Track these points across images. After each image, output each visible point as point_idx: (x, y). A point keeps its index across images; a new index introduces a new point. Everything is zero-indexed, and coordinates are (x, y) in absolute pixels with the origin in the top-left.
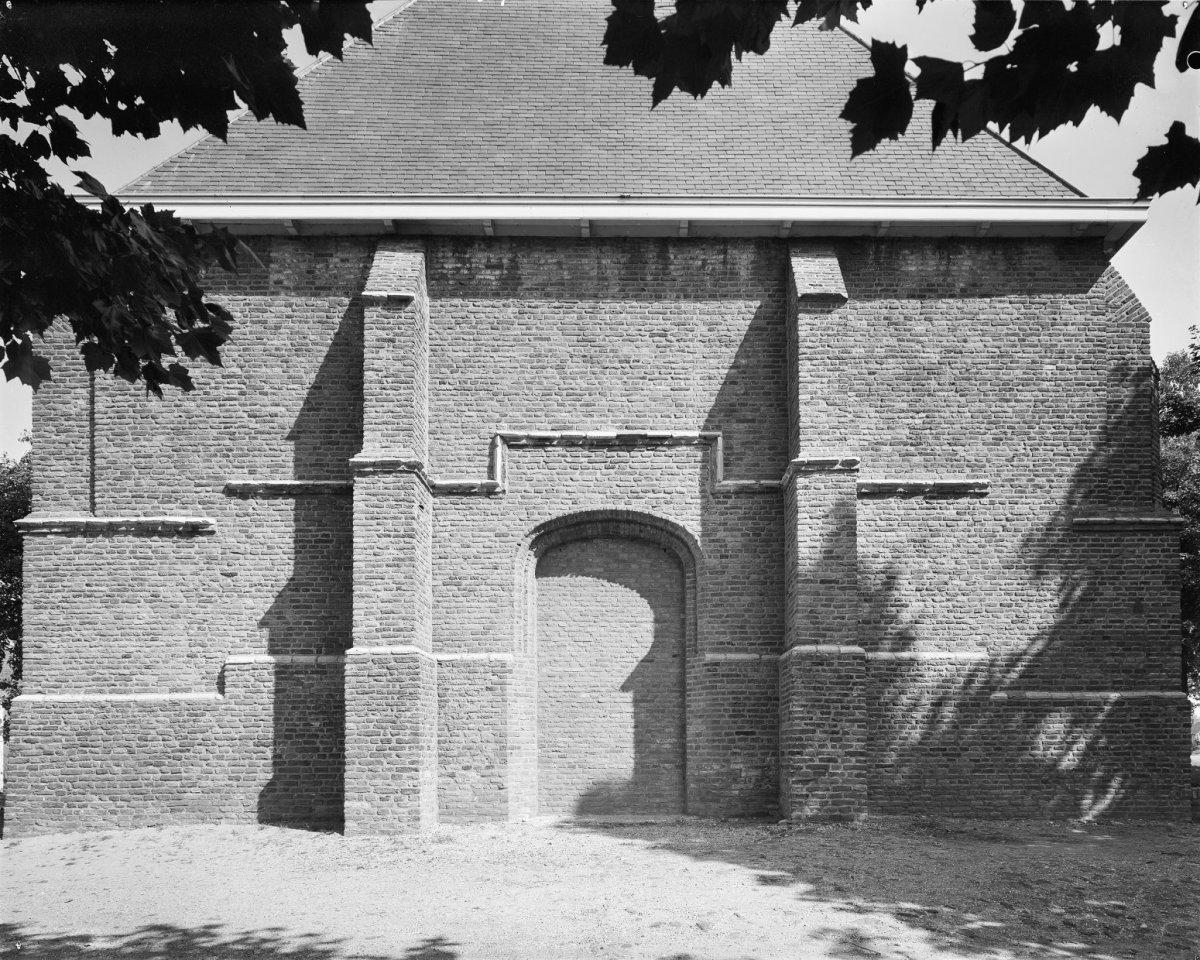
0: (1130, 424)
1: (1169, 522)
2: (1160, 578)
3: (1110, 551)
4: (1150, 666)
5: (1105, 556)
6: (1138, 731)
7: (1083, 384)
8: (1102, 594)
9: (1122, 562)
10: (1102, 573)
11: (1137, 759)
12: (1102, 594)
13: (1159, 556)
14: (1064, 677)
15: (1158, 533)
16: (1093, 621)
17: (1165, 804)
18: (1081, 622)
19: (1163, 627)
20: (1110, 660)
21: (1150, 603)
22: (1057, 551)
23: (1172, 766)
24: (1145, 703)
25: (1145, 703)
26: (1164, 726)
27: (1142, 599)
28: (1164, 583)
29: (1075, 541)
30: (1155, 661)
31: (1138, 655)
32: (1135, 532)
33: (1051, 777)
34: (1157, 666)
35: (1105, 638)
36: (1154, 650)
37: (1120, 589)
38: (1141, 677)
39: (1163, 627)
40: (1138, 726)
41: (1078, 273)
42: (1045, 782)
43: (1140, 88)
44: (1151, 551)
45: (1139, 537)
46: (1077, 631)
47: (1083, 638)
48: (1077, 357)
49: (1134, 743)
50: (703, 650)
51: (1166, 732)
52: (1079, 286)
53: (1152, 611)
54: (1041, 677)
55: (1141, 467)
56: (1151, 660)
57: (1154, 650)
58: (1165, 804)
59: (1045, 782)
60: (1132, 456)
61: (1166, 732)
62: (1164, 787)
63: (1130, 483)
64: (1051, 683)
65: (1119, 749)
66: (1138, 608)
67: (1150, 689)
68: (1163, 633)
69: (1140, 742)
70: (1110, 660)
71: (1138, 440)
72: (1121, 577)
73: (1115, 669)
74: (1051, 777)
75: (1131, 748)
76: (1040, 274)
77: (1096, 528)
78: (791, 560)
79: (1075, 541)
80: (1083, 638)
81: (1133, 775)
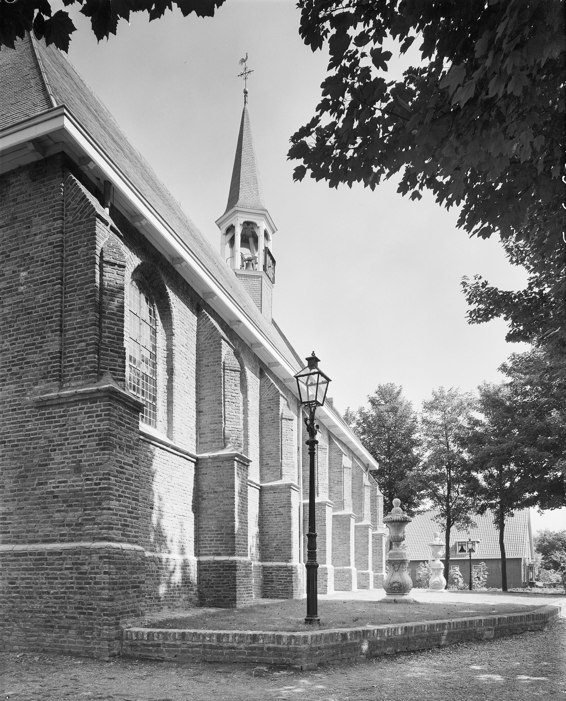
0: (80, 309)
1: (98, 391)
2: (95, 440)
3: (59, 421)
4: (86, 520)
5: (56, 427)
6: (72, 578)
7: (45, 282)
8: (53, 459)
9: (67, 430)
10: (53, 441)
11: (69, 603)
12: (53, 459)
13: (94, 421)
14: (28, 532)
15: (93, 401)
16: (46, 483)
17: (89, 643)
18: (39, 484)
19: (96, 484)
20: (58, 516)
21: (87, 463)
22: (24, 426)
23: (94, 609)
24: (76, 553)
25: (76, 553)
26: (90, 573)
27: (81, 461)
28: (97, 445)
29: (36, 416)
30: (89, 515)
31: (77, 511)
32: (76, 402)
33: (10, 616)
34: (90, 520)
35: (55, 497)
36: (89, 505)
37: (66, 453)
38: (79, 530)
39: (96, 484)
40: (71, 573)
41: (44, 190)
42: (6, 620)
43: (70, 41)
44: (89, 417)
45: (80, 406)
46: (36, 492)
47: (40, 498)
48: (43, 260)
49: (67, 588)
50: (441, 425)
51: (91, 578)
52: (45, 200)
53: (88, 471)
54: (13, 533)
55: (88, 345)
56: (86, 515)
57: (89, 505)
58: (89, 643)
59: (6, 620)
60: (81, 337)
61: (91, 578)
62: (88, 629)
63: (79, 360)
64: (18, 537)
65: (57, 593)
66: (78, 470)
67: (85, 541)
68: (96, 489)
69: (72, 588)
70: (58, 516)
71: (86, 321)
72: (66, 442)
73: (62, 524)
74: (10, 616)
75: (65, 593)
76: (20, 198)
77: (49, 403)
78: (194, 311)
79: (36, 416)
80: (40, 498)
81: (67, 617)
